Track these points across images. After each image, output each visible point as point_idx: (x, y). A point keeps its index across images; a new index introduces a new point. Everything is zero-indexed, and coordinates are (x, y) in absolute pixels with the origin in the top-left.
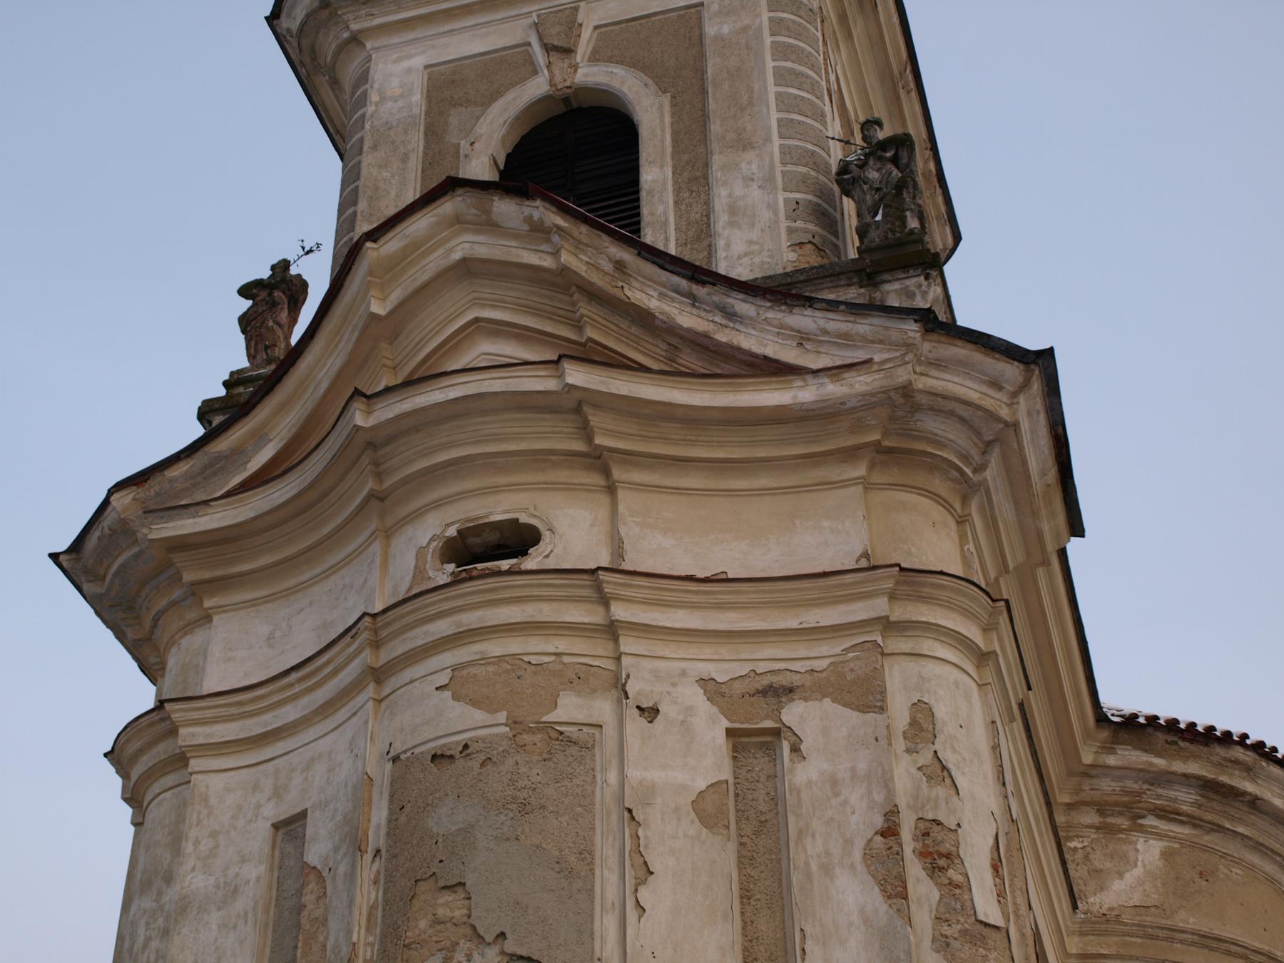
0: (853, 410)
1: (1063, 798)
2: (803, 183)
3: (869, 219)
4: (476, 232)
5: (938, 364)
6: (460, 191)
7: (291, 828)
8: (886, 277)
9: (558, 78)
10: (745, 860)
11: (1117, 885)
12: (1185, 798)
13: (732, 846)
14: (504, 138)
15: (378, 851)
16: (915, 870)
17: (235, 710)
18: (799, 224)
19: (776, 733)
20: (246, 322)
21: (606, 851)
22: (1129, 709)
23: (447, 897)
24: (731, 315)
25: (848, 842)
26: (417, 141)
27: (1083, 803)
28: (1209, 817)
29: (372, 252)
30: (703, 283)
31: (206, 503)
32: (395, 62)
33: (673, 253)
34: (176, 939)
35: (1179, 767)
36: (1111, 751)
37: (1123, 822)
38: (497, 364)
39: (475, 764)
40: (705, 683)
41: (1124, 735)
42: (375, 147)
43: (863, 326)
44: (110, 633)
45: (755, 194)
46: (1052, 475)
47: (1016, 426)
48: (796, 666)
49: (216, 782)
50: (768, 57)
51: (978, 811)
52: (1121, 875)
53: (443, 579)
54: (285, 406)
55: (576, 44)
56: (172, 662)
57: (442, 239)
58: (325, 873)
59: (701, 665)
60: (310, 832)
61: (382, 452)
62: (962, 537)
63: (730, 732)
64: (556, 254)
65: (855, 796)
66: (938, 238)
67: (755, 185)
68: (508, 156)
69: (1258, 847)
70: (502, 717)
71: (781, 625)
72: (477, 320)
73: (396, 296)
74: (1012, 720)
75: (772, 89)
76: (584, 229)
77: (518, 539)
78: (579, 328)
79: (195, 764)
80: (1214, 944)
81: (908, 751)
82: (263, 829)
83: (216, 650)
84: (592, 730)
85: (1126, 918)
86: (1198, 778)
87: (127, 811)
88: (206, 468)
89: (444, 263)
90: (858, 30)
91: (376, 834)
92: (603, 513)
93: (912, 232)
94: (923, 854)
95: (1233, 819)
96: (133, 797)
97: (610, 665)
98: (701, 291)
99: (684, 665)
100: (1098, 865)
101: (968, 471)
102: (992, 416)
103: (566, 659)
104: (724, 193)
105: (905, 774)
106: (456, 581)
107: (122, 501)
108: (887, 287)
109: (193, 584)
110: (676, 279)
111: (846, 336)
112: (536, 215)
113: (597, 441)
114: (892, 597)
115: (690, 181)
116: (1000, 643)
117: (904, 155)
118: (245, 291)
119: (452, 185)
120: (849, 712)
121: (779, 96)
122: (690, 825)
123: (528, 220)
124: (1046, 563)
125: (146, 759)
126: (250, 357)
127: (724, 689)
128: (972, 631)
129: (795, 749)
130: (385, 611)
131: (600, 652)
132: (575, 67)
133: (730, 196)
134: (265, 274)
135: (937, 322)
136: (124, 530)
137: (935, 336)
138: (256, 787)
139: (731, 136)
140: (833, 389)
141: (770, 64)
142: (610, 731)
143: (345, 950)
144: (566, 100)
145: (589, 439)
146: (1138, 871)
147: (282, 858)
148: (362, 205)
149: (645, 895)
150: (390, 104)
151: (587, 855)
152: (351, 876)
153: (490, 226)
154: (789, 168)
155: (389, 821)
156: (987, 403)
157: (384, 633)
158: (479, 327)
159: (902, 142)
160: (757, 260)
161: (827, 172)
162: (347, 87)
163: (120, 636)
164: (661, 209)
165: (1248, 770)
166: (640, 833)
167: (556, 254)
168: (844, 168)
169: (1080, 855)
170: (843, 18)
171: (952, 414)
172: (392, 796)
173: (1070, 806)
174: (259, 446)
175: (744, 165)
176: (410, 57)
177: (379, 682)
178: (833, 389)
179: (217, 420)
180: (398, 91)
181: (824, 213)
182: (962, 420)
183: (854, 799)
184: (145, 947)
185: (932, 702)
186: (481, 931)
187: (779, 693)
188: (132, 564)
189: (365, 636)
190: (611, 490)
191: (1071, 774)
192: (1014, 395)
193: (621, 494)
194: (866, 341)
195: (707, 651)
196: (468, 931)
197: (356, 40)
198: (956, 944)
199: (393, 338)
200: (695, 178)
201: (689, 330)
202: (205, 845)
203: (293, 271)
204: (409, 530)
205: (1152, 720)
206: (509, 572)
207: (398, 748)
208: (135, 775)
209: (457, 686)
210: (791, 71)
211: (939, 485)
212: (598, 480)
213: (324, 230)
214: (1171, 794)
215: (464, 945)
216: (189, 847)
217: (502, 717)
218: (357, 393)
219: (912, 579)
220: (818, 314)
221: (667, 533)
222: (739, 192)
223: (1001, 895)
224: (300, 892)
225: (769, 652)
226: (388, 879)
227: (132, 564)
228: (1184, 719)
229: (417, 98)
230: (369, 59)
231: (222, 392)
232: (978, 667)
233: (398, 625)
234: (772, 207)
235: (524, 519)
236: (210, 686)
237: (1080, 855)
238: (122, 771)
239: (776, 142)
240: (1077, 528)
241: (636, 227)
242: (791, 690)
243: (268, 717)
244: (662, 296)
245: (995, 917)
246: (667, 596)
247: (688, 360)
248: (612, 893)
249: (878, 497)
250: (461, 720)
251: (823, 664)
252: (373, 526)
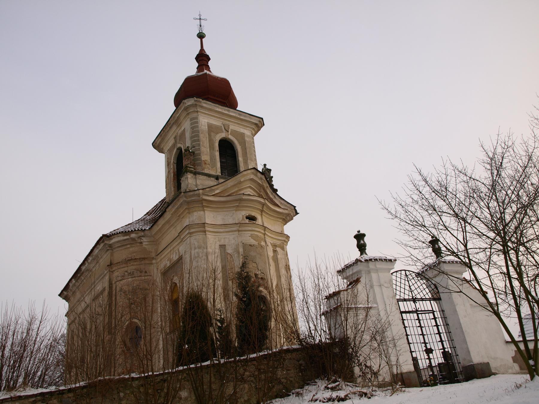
24: (275, 197)
153: (256, 175)
158: (250, 187)
209: (252, 236)
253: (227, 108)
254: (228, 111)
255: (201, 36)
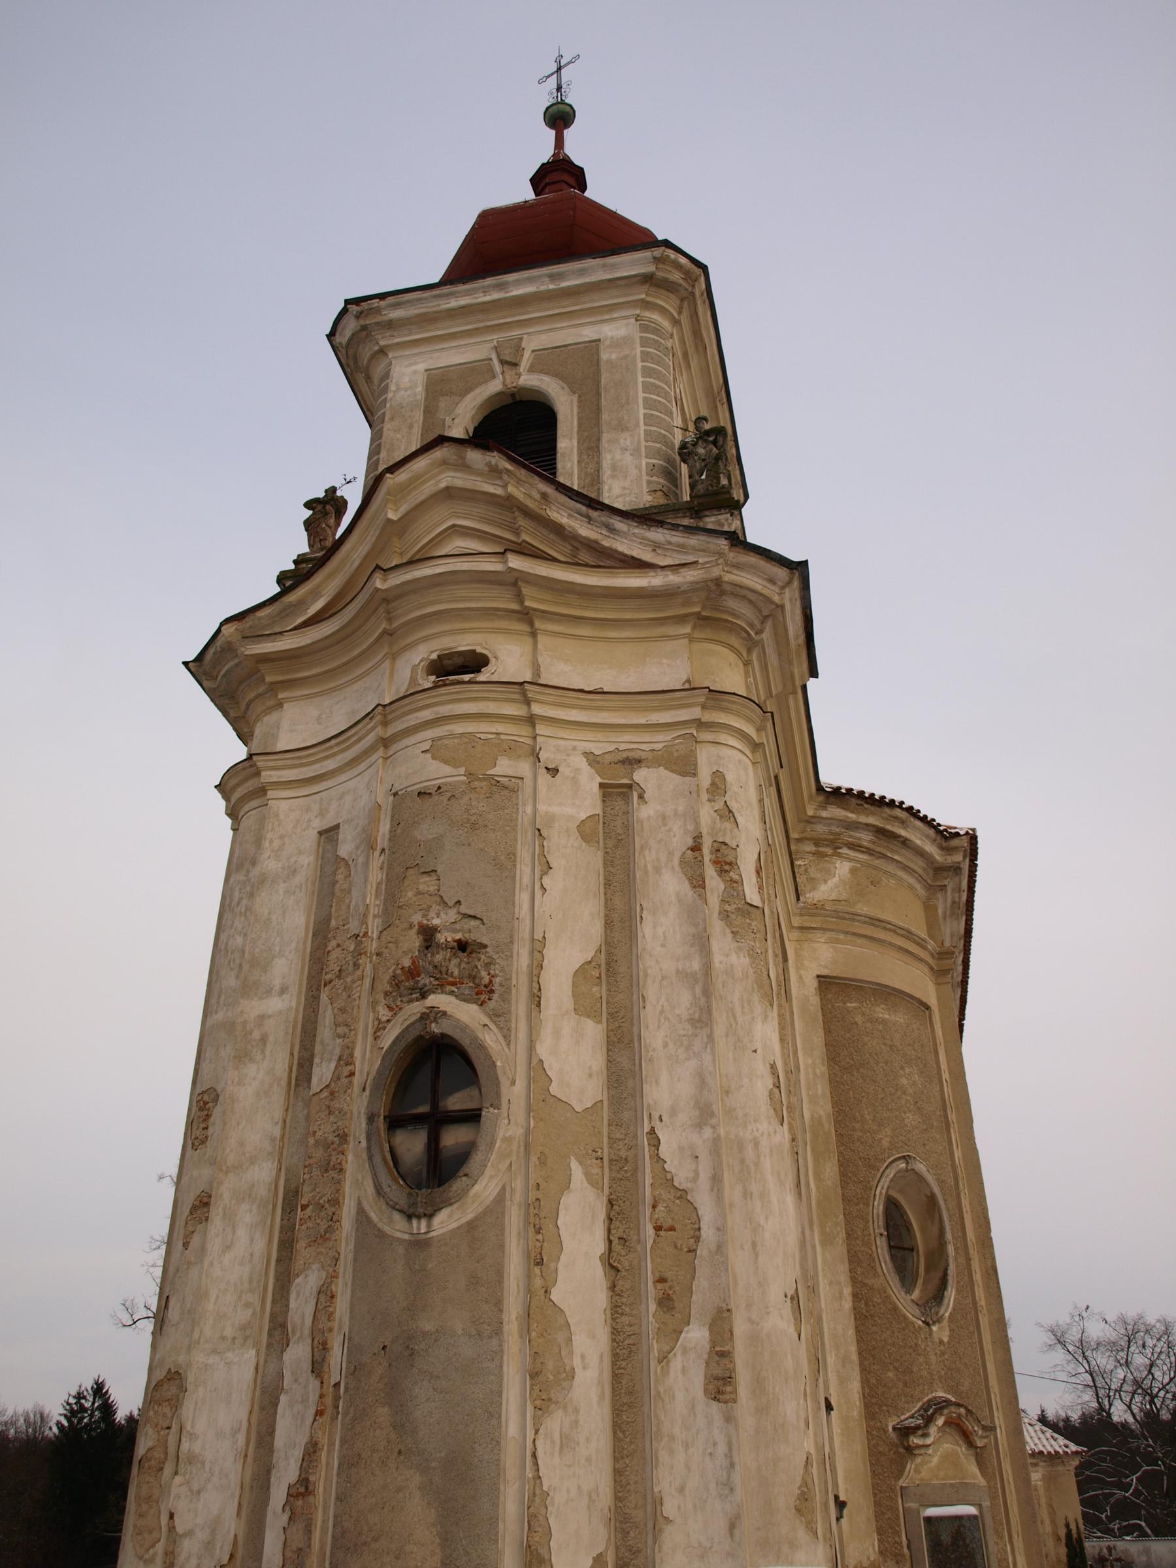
0: (685, 592)
1: (794, 835)
2: (658, 454)
3: (697, 478)
4: (455, 470)
5: (738, 566)
6: (446, 444)
7: (329, 834)
8: (707, 513)
9: (508, 381)
10: (608, 862)
11: (823, 888)
12: (865, 838)
13: (600, 854)
14: (473, 417)
15: (383, 849)
16: (710, 872)
17: (296, 762)
18: (655, 479)
19: (630, 787)
20: (308, 524)
21: (524, 854)
22: (836, 784)
23: (425, 879)
24: (612, 530)
25: (671, 853)
26: (419, 416)
27: (806, 839)
28: (878, 849)
29: (390, 480)
30: (596, 509)
31: (281, 633)
32: (407, 366)
33: (576, 488)
34: (258, 899)
35: (863, 819)
36: (825, 808)
37: (829, 851)
38: (468, 554)
39: (445, 798)
40: (587, 754)
41: (832, 799)
42: (392, 419)
43: (694, 541)
44: (220, 714)
45: (628, 458)
46: (802, 639)
47: (782, 607)
48: (643, 747)
49: (284, 806)
50: (639, 375)
51: (750, 838)
52: (825, 882)
53: (428, 685)
54: (331, 576)
55: (520, 360)
56: (258, 731)
57: (435, 474)
58: (350, 862)
59: (584, 744)
60: (341, 837)
61: (393, 604)
62: (747, 674)
63: (601, 785)
64: (505, 486)
65: (676, 826)
66: (737, 494)
67: (628, 453)
68: (475, 428)
69: (906, 868)
70: (462, 770)
71: (635, 721)
72: (454, 526)
73: (403, 509)
74: (771, 785)
75: (641, 395)
76: (523, 472)
77: (475, 663)
78: (518, 534)
79: (271, 794)
80: (877, 923)
81: (709, 800)
82: (312, 834)
83: (285, 724)
84: (517, 781)
85: (827, 907)
86: (873, 826)
87: (229, 821)
88: (281, 612)
89: (434, 489)
90: (694, 363)
91: (382, 840)
92: (528, 648)
93: (723, 487)
94: (715, 862)
95: (892, 851)
96: (232, 813)
97: (529, 741)
98: (594, 514)
99: (575, 743)
100: (813, 875)
101: (752, 633)
102: (768, 600)
103: (503, 737)
104: (609, 457)
105: (706, 814)
106: (436, 686)
107: (228, 630)
108: (707, 519)
109: (272, 683)
110: (579, 506)
111: (682, 546)
112: (493, 461)
113: (527, 603)
114: (704, 707)
115: (588, 448)
116: (767, 739)
117: (720, 439)
118: (308, 505)
119: (442, 440)
120: (674, 776)
121: (645, 399)
122: (575, 840)
123: (489, 464)
124: (794, 693)
125: (241, 789)
126: (311, 546)
127: (598, 759)
128: (750, 730)
129: (641, 797)
130: (391, 703)
131: (524, 733)
132: (519, 375)
133: (613, 459)
134: (321, 495)
135: (737, 540)
136: (229, 648)
137: (737, 549)
138: (308, 809)
139: (614, 422)
140: (673, 578)
141: (640, 380)
142: (528, 782)
143: (362, 909)
144: (513, 395)
145: (521, 602)
146: (836, 880)
147: (324, 852)
148: (383, 454)
149: (546, 881)
150: (402, 392)
151: (512, 856)
152: (366, 864)
153: (464, 467)
154: (650, 444)
155: (391, 832)
156: (766, 592)
157: (390, 717)
158: (456, 531)
159: (719, 432)
160: (628, 499)
161: (672, 448)
162: (376, 381)
163: (225, 714)
164: (569, 465)
165: (903, 822)
166: (545, 843)
167: (505, 486)
168: (683, 446)
169: (803, 868)
170: (685, 355)
171: (744, 597)
172: (392, 817)
173: (798, 840)
174: (314, 600)
175: (622, 441)
176: (416, 363)
177: (386, 747)
178: (673, 578)
179: (288, 583)
180: (408, 385)
181: (670, 473)
182: (750, 601)
183: (675, 828)
184: (238, 904)
185: (725, 772)
186: (446, 899)
187: (633, 763)
188: (232, 671)
189: (378, 718)
190: (534, 634)
191: (800, 821)
192: (783, 588)
193: (540, 637)
194: (696, 550)
195: (590, 736)
196: (438, 899)
197: (382, 351)
198: (733, 916)
199: (401, 534)
200: (591, 447)
201: (586, 538)
202: (276, 843)
203: (339, 493)
204: (407, 655)
205: (850, 790)
206: (469, 682)
207: (397, 788)
208: (233, 799)
209: (435, 750)
210: (653, 385)
211: (734, 641)
212: (525, 628)
213: (358, 468)
214: (858, 835)
215: (435, 908)
216: (266, 844)
217: (462, 770)
218: (378, 567)
219: (716, 697)
220: (666, 531)
221: (568, 662)
222: (618, 456)
223: (760, 888)
224: (334, 873)
225: (627, 738)
226: (389, 867)
227: (232, 671)
228: (868, 791)
229: (420, 389)
230: (390, 364)
231: (292, 567)
232: (753, 752)
233: (397, 713)
234: (638, 467)
235: (479, 650)
236: (281, 746)
237: (803, 868)
238: (226, 795)
239: (642, 427)
240: (814, 673)
241: (554, 474)
242: (640, 761)
243: (317, 766)
244: (570, 516)
245: (756, 901)
246: (566, 701)
247: (584, 556)
248: (526, 880)
249: (697, 646)
250: (436, 772)
251: (660, 746)
252: (385, 651)
253: (489, 281)
254: (501, 287)
255: (560, 118)
